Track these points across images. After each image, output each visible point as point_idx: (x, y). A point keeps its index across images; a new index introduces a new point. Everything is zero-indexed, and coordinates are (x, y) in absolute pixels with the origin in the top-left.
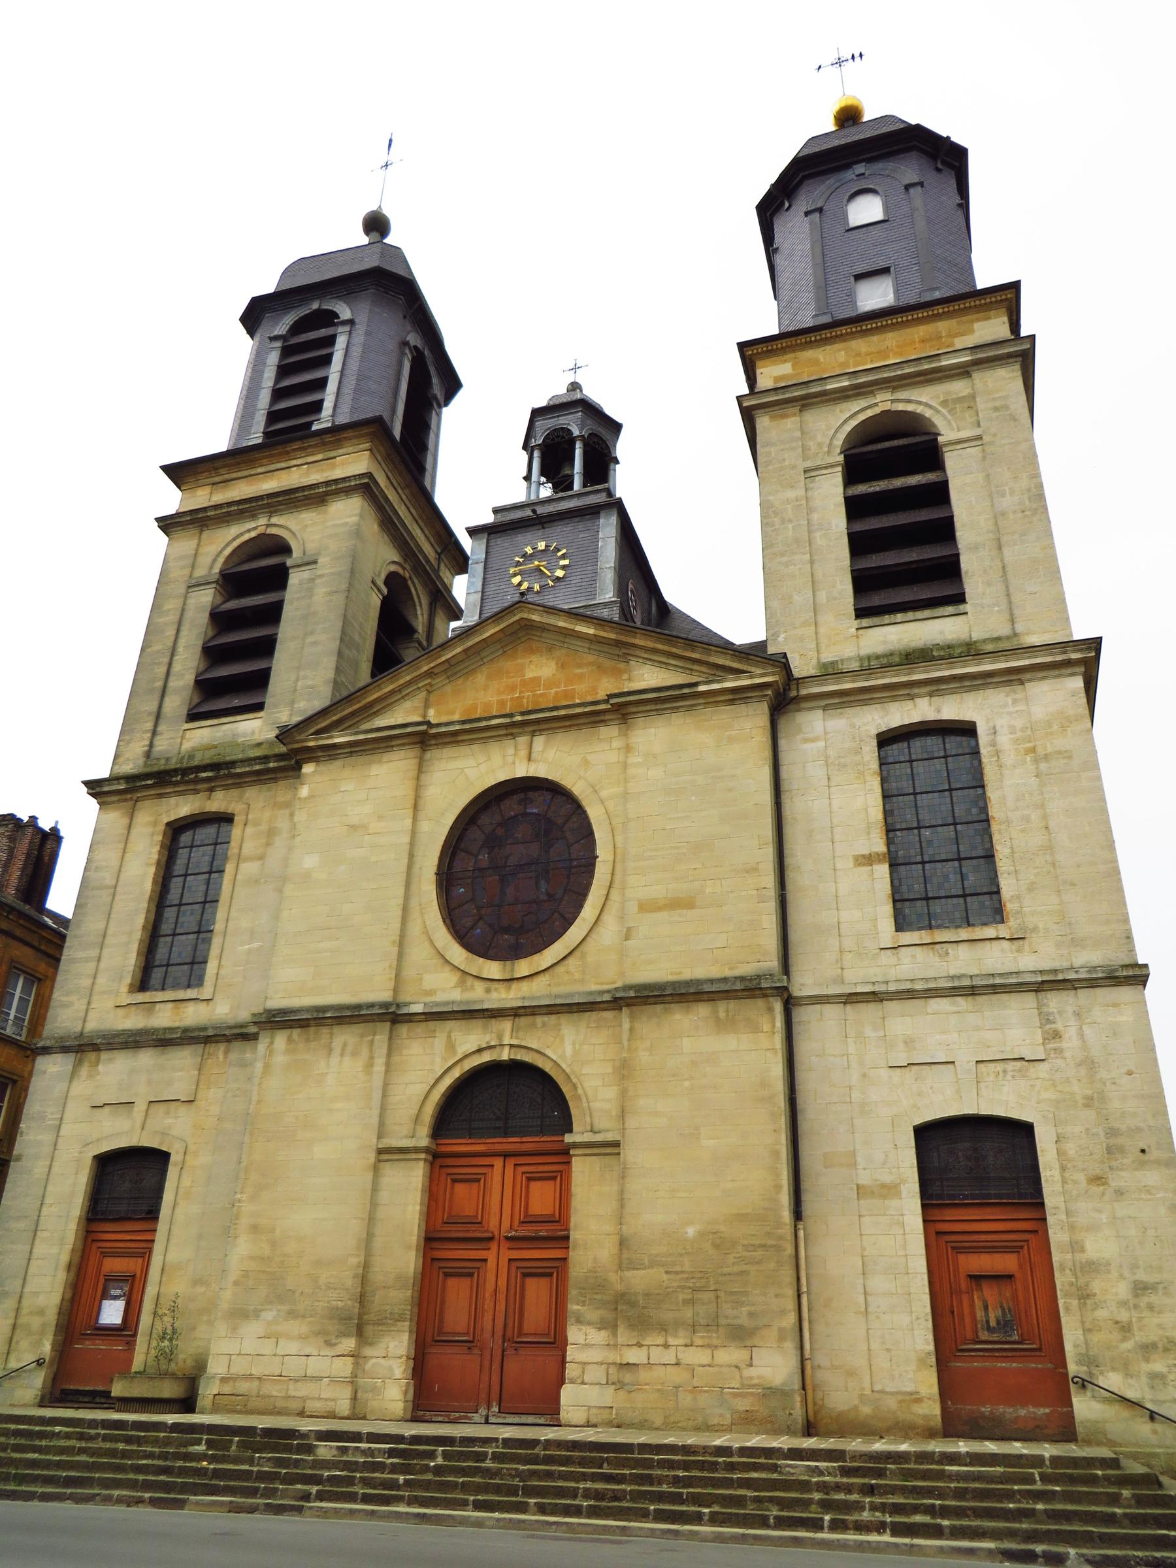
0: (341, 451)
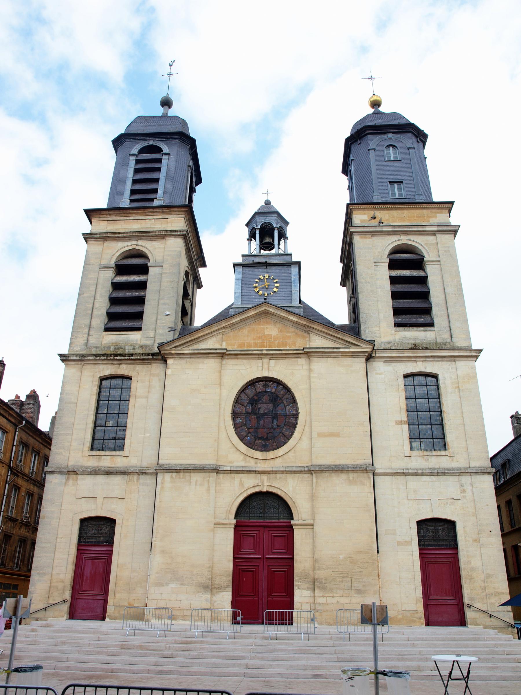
0: (171, 216)
